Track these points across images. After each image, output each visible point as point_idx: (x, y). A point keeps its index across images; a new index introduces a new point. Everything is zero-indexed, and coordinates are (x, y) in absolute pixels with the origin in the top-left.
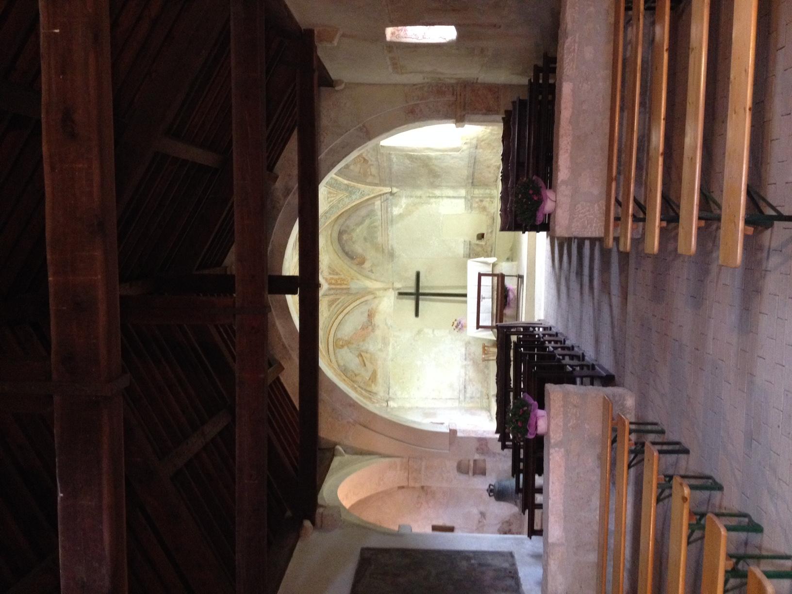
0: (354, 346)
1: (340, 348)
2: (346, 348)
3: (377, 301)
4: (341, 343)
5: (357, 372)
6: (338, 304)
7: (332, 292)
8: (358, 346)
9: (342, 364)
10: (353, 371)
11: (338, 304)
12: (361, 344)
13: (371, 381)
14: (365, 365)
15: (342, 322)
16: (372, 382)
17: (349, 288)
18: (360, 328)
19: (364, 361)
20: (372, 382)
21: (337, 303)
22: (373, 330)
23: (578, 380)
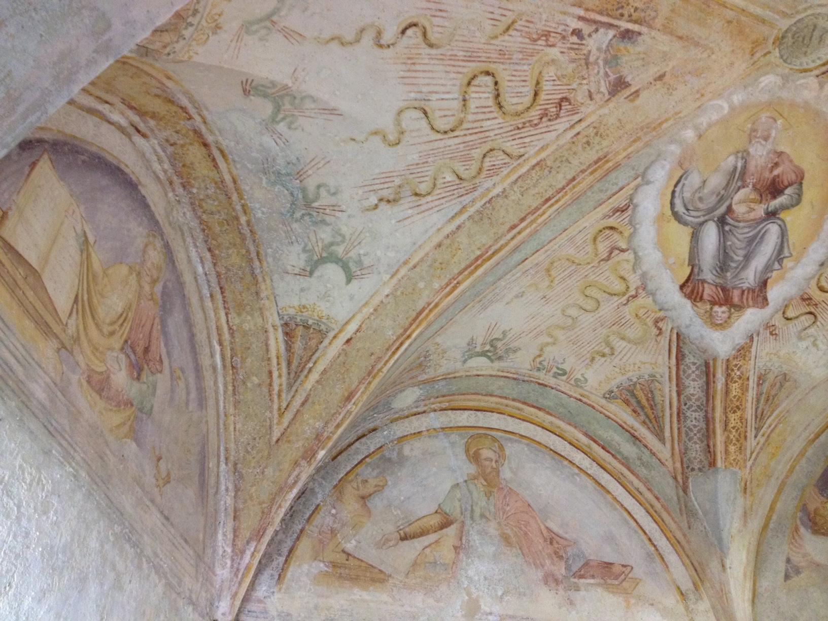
0: (482, 503)
1: (467, 451)
2: (472, 469)
3: (671, 600)
4: (486, 453)
5: (377, 504)
6: (635, 438)
7: (694, 387)
8: (482, 516)
9: (407, 451)
10: (380, 489)
11: (635, 438)
12: (492, 529)
13: (341, 558)
14: (404, 538)
15: (566, 463)
16: (335, 565)
17: (713, 464)
18: (556, 529)
19: (423, 533)
20: (335, 565)
21: (643, 432)
22: (550, 580)
23: (583, 589)
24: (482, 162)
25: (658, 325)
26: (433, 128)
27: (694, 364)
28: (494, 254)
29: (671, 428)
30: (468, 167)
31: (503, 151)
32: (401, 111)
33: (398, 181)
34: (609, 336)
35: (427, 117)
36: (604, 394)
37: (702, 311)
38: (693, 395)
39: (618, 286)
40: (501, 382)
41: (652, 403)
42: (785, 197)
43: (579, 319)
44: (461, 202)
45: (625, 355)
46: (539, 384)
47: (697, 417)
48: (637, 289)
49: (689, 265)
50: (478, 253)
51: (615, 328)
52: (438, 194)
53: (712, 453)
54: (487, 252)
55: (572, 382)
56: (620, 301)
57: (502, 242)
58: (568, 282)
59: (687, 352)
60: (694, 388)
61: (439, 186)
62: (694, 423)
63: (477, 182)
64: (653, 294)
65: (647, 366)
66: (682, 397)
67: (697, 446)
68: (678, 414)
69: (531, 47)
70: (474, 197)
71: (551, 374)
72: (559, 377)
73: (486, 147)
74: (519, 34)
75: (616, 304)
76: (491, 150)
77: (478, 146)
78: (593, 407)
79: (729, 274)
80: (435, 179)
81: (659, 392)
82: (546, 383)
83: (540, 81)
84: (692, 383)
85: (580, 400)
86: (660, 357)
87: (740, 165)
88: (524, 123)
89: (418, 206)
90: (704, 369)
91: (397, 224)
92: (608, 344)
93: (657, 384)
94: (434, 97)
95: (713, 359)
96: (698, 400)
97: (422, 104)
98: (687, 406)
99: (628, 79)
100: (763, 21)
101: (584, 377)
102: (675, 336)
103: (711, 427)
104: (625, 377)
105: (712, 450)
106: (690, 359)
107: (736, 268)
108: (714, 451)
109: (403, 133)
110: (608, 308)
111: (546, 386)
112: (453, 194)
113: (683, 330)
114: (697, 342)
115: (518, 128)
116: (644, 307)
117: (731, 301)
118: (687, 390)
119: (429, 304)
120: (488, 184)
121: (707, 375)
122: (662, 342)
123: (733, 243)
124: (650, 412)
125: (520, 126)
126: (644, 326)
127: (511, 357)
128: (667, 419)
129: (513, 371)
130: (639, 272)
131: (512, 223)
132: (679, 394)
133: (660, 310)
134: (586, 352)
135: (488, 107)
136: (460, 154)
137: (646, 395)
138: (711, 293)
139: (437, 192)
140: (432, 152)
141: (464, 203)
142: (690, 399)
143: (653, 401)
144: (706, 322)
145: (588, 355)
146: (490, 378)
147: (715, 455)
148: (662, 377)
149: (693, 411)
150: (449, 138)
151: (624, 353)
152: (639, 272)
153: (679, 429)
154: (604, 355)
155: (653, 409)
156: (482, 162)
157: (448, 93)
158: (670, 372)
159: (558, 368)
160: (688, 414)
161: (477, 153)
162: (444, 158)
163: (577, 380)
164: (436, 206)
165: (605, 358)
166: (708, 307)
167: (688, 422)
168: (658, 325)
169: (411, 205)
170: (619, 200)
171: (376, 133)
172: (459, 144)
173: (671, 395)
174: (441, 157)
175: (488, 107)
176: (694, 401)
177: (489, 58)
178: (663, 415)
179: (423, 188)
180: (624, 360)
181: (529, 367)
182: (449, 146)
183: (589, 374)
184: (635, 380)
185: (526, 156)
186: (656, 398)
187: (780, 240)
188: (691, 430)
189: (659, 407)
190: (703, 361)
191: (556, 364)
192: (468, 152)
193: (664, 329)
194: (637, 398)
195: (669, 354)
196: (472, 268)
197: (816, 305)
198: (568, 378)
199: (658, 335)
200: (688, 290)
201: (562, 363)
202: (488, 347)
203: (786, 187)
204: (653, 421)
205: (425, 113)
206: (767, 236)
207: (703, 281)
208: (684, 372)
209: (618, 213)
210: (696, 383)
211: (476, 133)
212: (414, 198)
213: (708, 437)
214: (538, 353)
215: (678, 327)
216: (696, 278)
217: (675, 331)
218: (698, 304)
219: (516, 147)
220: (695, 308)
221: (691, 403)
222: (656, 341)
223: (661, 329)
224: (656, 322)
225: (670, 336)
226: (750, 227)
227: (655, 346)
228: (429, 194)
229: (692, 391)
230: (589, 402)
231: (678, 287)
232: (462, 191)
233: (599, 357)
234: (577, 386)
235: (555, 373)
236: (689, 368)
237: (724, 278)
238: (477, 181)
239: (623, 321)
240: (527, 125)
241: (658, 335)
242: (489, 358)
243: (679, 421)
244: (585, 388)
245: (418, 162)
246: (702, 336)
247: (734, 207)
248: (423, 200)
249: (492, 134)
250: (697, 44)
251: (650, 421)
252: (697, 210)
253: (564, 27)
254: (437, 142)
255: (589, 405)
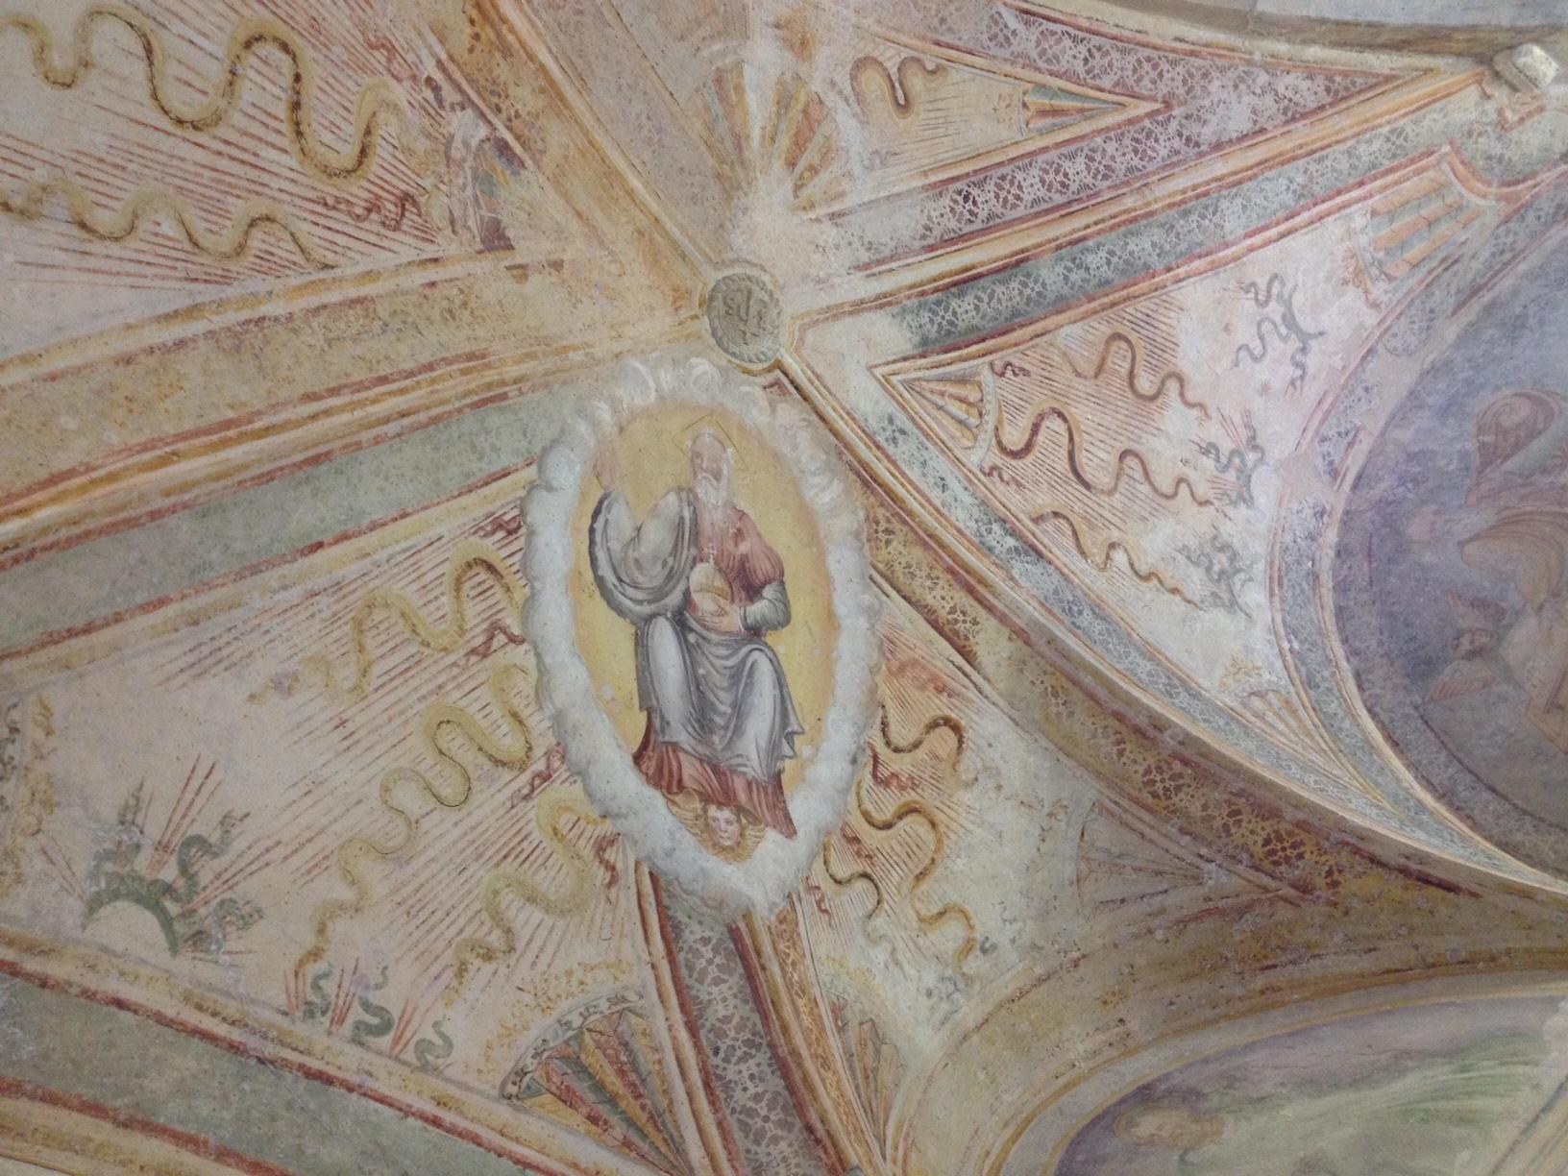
24: (247, 233)
25: (606, 856)
26: (155, 96)
27: (706, 941)
28: (267, 431)
29: (701, 1131)
30: (215, 228)
31: (292, 235)
32: (100, 13)
33: (41, 174)
34: (496, 893)
35: (151, 64)
36: (503, 1085)
37: (690, 815)
38: (726, 1020)
39: (509, 743)
40: (189, 1060)
41: (633, 1077)
42: (765, 602)
43: (425, 824)
44: (190, 294)
45: (542, 949)
46: (310, 1074)
47: (755, 1070)
48: (548, 754)
49: (641, 708)
50: (231, 414)
51: (509, 867)
52: (137, 251)
53: (829, 1145)
54: (250, 422)
55: (410, 1055)
56: (515, 786)
57: (283, 416)
58: (401, 693)
59: (681, 917)
60: (724, 1000)
61: (140, 233)
62: (752, 1090)
63: (233, 269)
64: (580, 773)
65: (602, 975)
66: (703, 1033)
67: (783, 1145)
68: (707, 1085)
69: (362, 50)
70: (223, 295)
71: (347, 1029)
72: (369, 1039)
73: (261, 208)
74: (348, 12)
75: (508, 792)
76: (268, 219)
77: (243, 194)
78: (476, 1140)
79: (716, 739)
80: (136, 216)
81: (644, 1041)
82: (332, 1071)
83: (373, 130)
84: (715, 989)
85: (436, 1122)
86: (627, 944)
87: (687, 514)
88: (338, 200)
89: (82, 253)
90: (732, 946)
91: (19, 267)
92: (498, 918)
93: (634, 1019)
94: (177, 27)
95: (744, 916)
96: (740, 1028)
97: (148, 25)
98: (722, 1054)
99: (510, 234)
100: (684, 257)
101: (442, 1036)
102: (647, 881)
103: (797, 1076)
104: (550, 1020)
105: (821, 1133)
106: (693, 933)
107: (726, 728)
108: (829, 1133)
109: (86, 65)
110: (492, 797)
111: (329, 1080)
112: (175, 268)
113: (662, 864)
114: (698, 887)
115: (326, 205)
116: (569, 809)
117: (735, 799)
118: (710, 1011)
119: (89, 468)
120: (259, 285)
121: (743, 958)
122: (623, 901)
123: (708, 673)
124: (631, 1105)
125: (330, 201)
126: (576, 862)
127: (230, 945)
128: (684, 1110)
129: (232, 1009)
130: (549, 710)
131: (309, 389)
132: (693, 1029)
133: (604, 817)
134: (441, 944)
135: (276, 118)
136: (201, 190)
137: (614, 1061)
138: (696, 775)
139: (132, 243)
140: (140, 151)
141: (199, 299)
142: (721, 1034)
143: (636, 1070)
144: (702, 841)
145: (449, 957)
146: (155, 1028)
147: (835, 1145)
148: (642, 997)
149: (741, 1060)
150: (184, 139)
151: (537, 943)
152: (549, 710)
153: (720, 1124)
154: (488, 956)
155: (640, 1096)
156: (247, 233)
157: (205, 35)
158: (657, 978)
159: (366, 1006)
160: (730, 1075)
161: (241, 209)
162: (162, 180)
163: (423, 1047)
164: (128, 275)
165: (493, 965)
166: (699, 806)
167: (738, 1094)
168: (606, 856)
169: (64, 242)
170: (499, 498)
171: (26, 26)
172: (204, 166)
173: (674, 1038)
174: (159, 176)
175: (276, 118)
176: (732, 1034)
177: (292, 17)
178: (671, 1103)
179: (102, 219)
180: (541, 967)
181: (281, 1001)
182: (183, 160)
183: (457, 1026)
184: (577, 1022)
185: (337, 272)
186: (641, 1059)
187: (777, 692)
188: (751, 1112)
189: (655, 1082)
190: (724, 929)
191: (360, 992)
192: (218, 196)
193: (619, 866)
194: (591, 1076)
195: (646, 932)
196: (214, 438)
197: (869, 857)
198: (396, 1042)
199: (610, 885)
200: (651, 766)
201: (378, 987)
202: (169, 873)
203: (764, 585)
204: (650, 1129)
205: (149, 50)
206: (757, 675)
207: (675, 747)
208: (690, 968)
209: (501, 534)
210: (724, 987)
211: (243, 162)
212: (75, 231)
213: (800, 1108)
214: (310, 940)
215: (648, 858)
216: (661, 738)
217: (646, 870)
218: (678, 799)
219: (317, 240)
220: (675, 809)
221: (729, 1042)
222: (609, 901)
223: (613, 868)
224: (601, 846)
225: (638, 883)
226: (727, 646)
227: (609, 917)
228: (117, 239)
229: (722, 1013)
230: (463, 1124)
231: (629, 761)
232: (195, 271)
233: (478, 962)
234: (424, 1068)
235: (358, 1026)
236: (698, 954)
237: (710, 744)
238: (234, 266)
239: (527, 847)
240: (342, 206)
241: (610, 885)
242: (167, 923)
243: (712, 1103)
244: (449, 1072)
245: (104, 155)
246: (703, 870)
247: (696, 597)
248: (97, 247)
249: (275, 183)
250: (602, 243)
251: (641, 1132)
252: (636, 586)
253: (415, 59)
254: (157, 134)
255: (462, 1134)
